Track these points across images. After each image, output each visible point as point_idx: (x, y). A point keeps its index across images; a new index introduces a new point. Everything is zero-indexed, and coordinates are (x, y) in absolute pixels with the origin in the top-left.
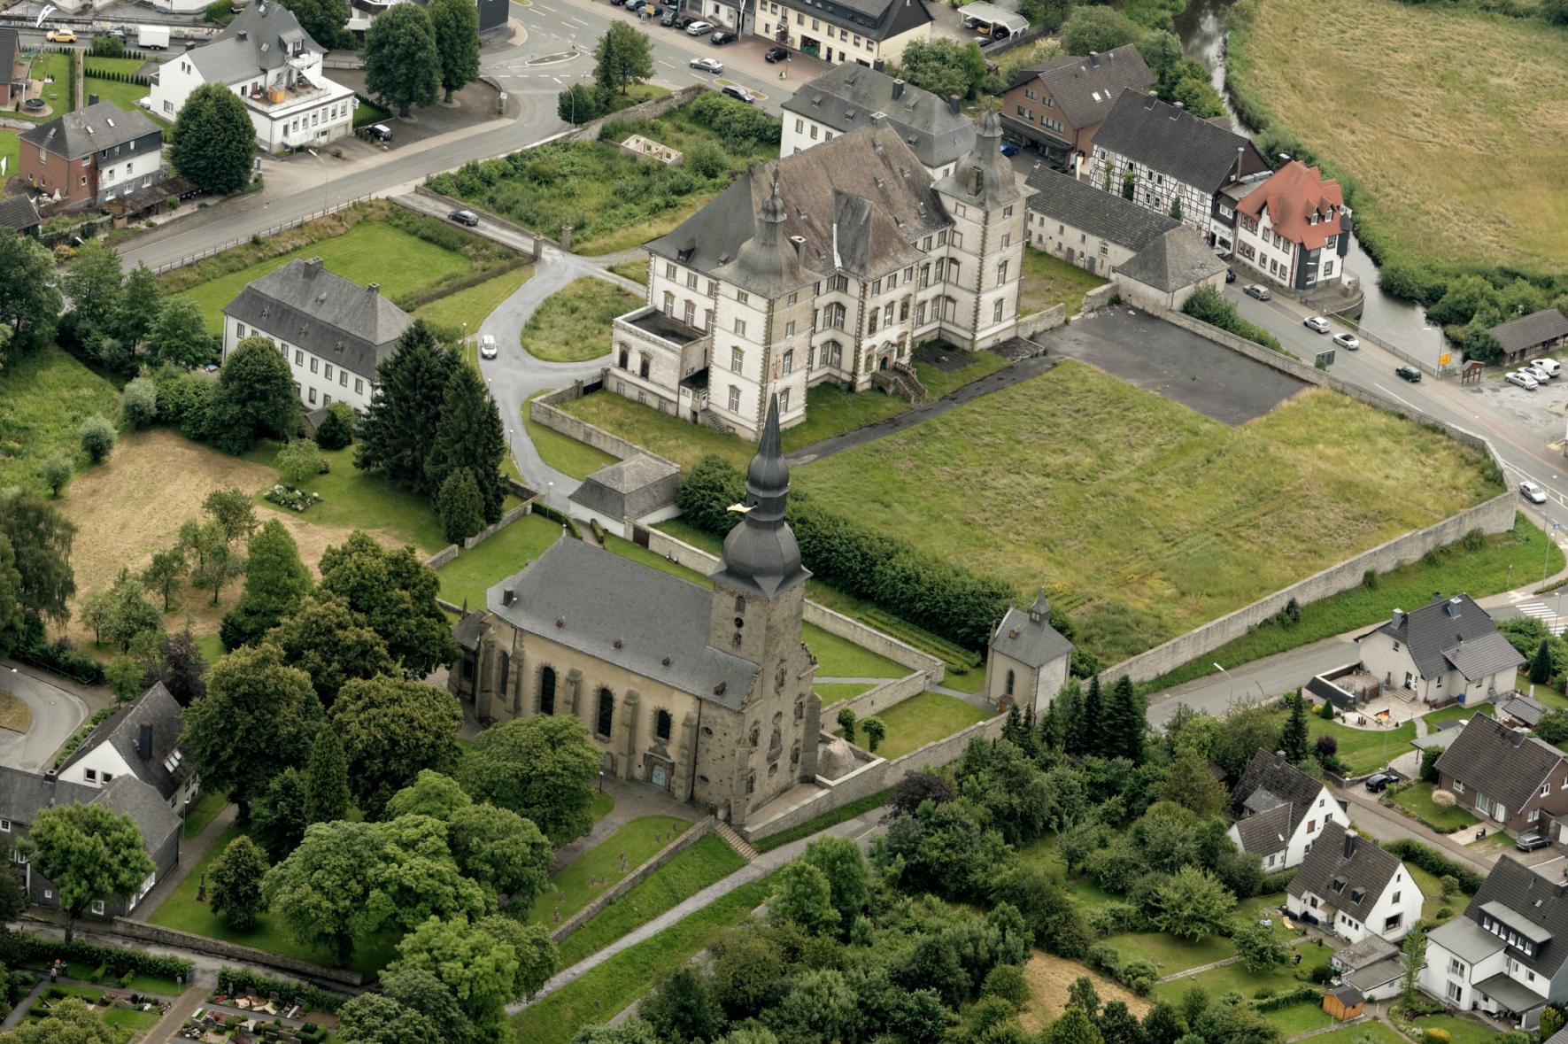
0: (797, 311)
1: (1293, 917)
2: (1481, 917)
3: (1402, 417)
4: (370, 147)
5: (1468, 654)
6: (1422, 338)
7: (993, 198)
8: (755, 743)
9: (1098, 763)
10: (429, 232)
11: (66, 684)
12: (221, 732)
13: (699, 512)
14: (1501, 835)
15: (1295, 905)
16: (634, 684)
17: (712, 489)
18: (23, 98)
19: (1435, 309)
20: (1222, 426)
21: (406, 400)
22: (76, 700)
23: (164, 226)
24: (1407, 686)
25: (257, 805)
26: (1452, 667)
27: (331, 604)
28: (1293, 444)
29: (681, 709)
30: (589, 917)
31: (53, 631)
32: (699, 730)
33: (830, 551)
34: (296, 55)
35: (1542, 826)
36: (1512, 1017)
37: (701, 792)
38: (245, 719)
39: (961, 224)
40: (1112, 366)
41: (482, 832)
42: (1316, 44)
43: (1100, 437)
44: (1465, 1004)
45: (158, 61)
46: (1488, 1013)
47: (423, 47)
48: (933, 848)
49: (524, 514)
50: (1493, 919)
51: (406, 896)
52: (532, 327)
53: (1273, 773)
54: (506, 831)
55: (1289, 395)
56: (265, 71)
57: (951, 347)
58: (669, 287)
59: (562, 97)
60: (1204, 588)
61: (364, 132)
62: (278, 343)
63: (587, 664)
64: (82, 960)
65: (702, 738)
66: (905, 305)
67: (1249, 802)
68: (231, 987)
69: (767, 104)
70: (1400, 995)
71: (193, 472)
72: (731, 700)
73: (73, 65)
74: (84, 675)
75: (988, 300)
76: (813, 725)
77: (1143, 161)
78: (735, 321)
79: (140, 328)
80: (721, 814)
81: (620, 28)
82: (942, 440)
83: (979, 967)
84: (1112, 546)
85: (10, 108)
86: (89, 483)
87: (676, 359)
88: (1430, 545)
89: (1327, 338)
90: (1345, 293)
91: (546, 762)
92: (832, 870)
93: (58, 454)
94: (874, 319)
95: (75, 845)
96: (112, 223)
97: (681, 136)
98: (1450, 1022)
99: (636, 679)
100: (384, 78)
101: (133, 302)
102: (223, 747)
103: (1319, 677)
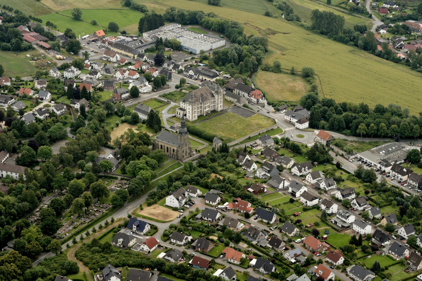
2: (263, 168)
6: (271, 109)
15: (243, 168)
28: (253, 120)
29: (175, 149)
31: (109, 143)
32: (177, 151)
40: (233, 112)
44: (261, 177)
48: (202, 162)
52: (169, 110)
58: (182, 105)
60: (240, 135)
61: (153, 91)
64: (106, 177)
68: (122, 179)
72: (180, 147)
75: (219, 105)
76: (191, 150)
78: (188, 107)
79: (123, 111)
81: (183, 78)
83: (204, 175)
86: (116, 128)
88: (267, 130)
91: (158, 154)
93: (112, 125)
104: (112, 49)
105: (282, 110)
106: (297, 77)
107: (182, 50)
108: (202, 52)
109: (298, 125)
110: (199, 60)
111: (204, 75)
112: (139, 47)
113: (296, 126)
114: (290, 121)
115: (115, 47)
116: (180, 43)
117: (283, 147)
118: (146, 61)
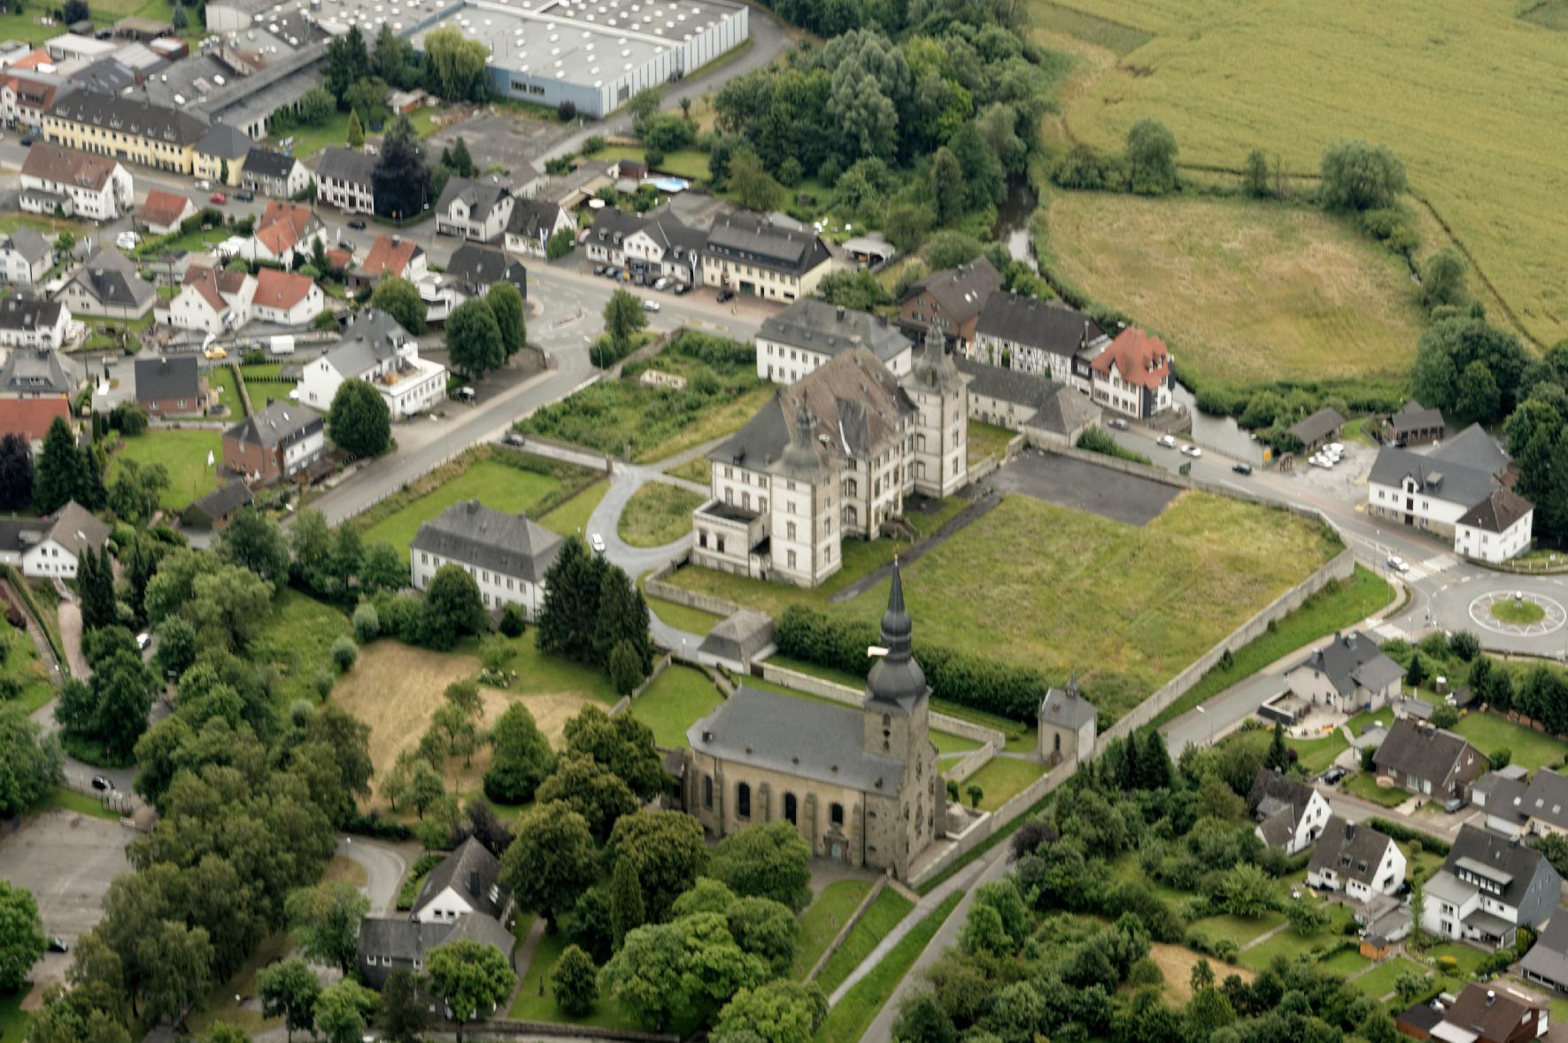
0: (831, 490)
1: (1315, 888)
2: (1457, 871)
3: (1255, 503)
4: (465, 407)
5: (1365, 673)
6: (1232, 439)
8: (907, 817)
9: (1145, 794)
10: (525, 464)
11: (382, 843)
12: (533, 870)
13: (794, 645)
14: (1431, 803)
15: (1315, 879)
16: (811, 787)
18: (208, 405)
19: (1243, 418)
20: (1134, 528)
21: (572, 596)
22: (394, 855)
25: (564, 921)
26: (1358, 684)
27: (582, 761)
29: (850, 801)
30: (824, 965)
32: (866, 814)
34: (400, 346)
35: (1458, 793)
36: (1493, 939)
37: (871, 858)
38: (550, 858)
39: (923, 409)
40: (1040, 494)
41: (750, 918)
42: (1095, 235)
43: (1052, 549)
44: (1456, 934)
46: (1474, 939)
47: (491, 328)
48: (1055, 876)
49: (666, 666)
50: (1465, 871)
51: (710, 975)
52: (623, 524)
53: (1275, 785)
54: (766, 914)
55: (1171, 498)
56: (380, 362)
57: (924, 498)
58: (728, 483)
59: (591, 351)
61: (455, 395)
62: (467, 568)
63: (772, 777)
65: (869, 819)
66: (896, 473)
67: (1261, 807)
69: (742, 338)
70: (1408, 935)
71: (418, 668)
72: (888, 789)
73: (234, 374)
74: (399, 836)
75: (948, 460)
82: (942, 567)
84: (1089, 628)
85: (200, 414)
87: (744, 535)
88: (1305, 595)
89: (1177, 452)
90: (1178, 416)
91: (776, 857)
92: (999, 906)
94: (877, 487)
95: (463, 974)
96: (300, 490)
97: (679, 366)
98: (1450, 949)
101: (345, 548)
102: (537, 880)
104: (50, 128)
105: (1316, 447)
106: (1297, 216)
107: (501, 100)
108: (644, 103)
109: (1474, 541)
110: (638, 157)
112: (229, 107)
113: (1459, 548)
114: (1409, 519)
115: (71, 117)
116: (481, 52)
117: (1473, 704)
118: (308, 194)
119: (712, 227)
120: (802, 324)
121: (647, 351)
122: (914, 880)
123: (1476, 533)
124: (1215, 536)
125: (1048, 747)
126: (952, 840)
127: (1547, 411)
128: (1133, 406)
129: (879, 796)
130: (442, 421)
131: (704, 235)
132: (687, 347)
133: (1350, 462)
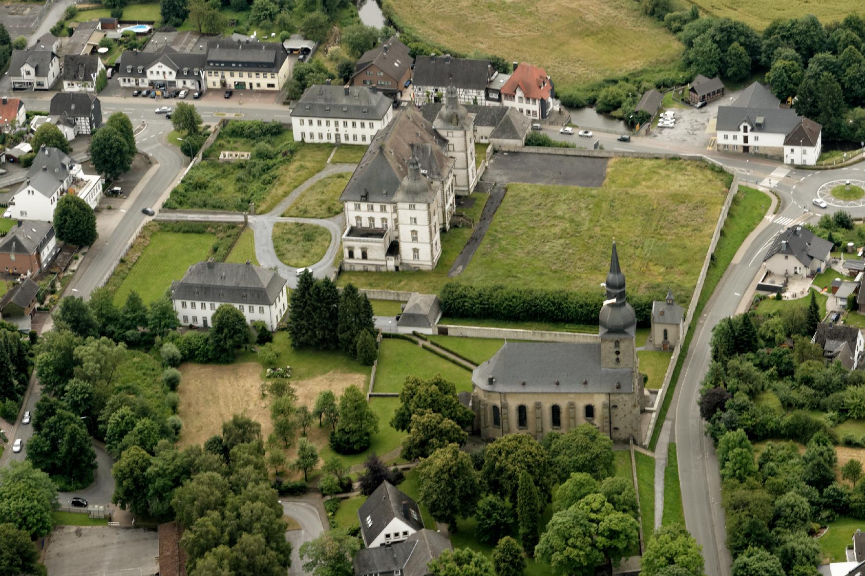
3: (657, 158)
7: (465, 124)
10: (186, 229)
16: (571, 398)
17: (461, 297)
22: (304, 504)
23: (78, 269)
24: (796, 273)
26: (812, 258)
29: (599, 402)
32: (611, 407)
33: (535, 306)
34: (71, 168)
39: (451, 141)
43: (560, 213)
45: (14, 193)
47: (124, 145)
55: (605, 166)
56: (62, 182)
58: (357, 213)
62: (237, 306)
63: (539, 398)
65: (612, 411)
72: (624, 389)
77: (443, 86)
80: (631, 442)
99: (572, 396)
100: (109, 165)
103: (760, 282)
111: (229, 66)
113: (787, 161)
114: (746, 149)
119: (208, 51)
120: (322, 102)
121: (211, 139)
122: (646, 443)
123: (798, 149)
124: (649, 184)
125: (658, 338)
126: (651, 412)
127: (793, 65)
128: (534, 113)
129: (619, 394)
130: (112, 212)
131: (204, 57)
132: (235, 132)
133: (681, 120)
